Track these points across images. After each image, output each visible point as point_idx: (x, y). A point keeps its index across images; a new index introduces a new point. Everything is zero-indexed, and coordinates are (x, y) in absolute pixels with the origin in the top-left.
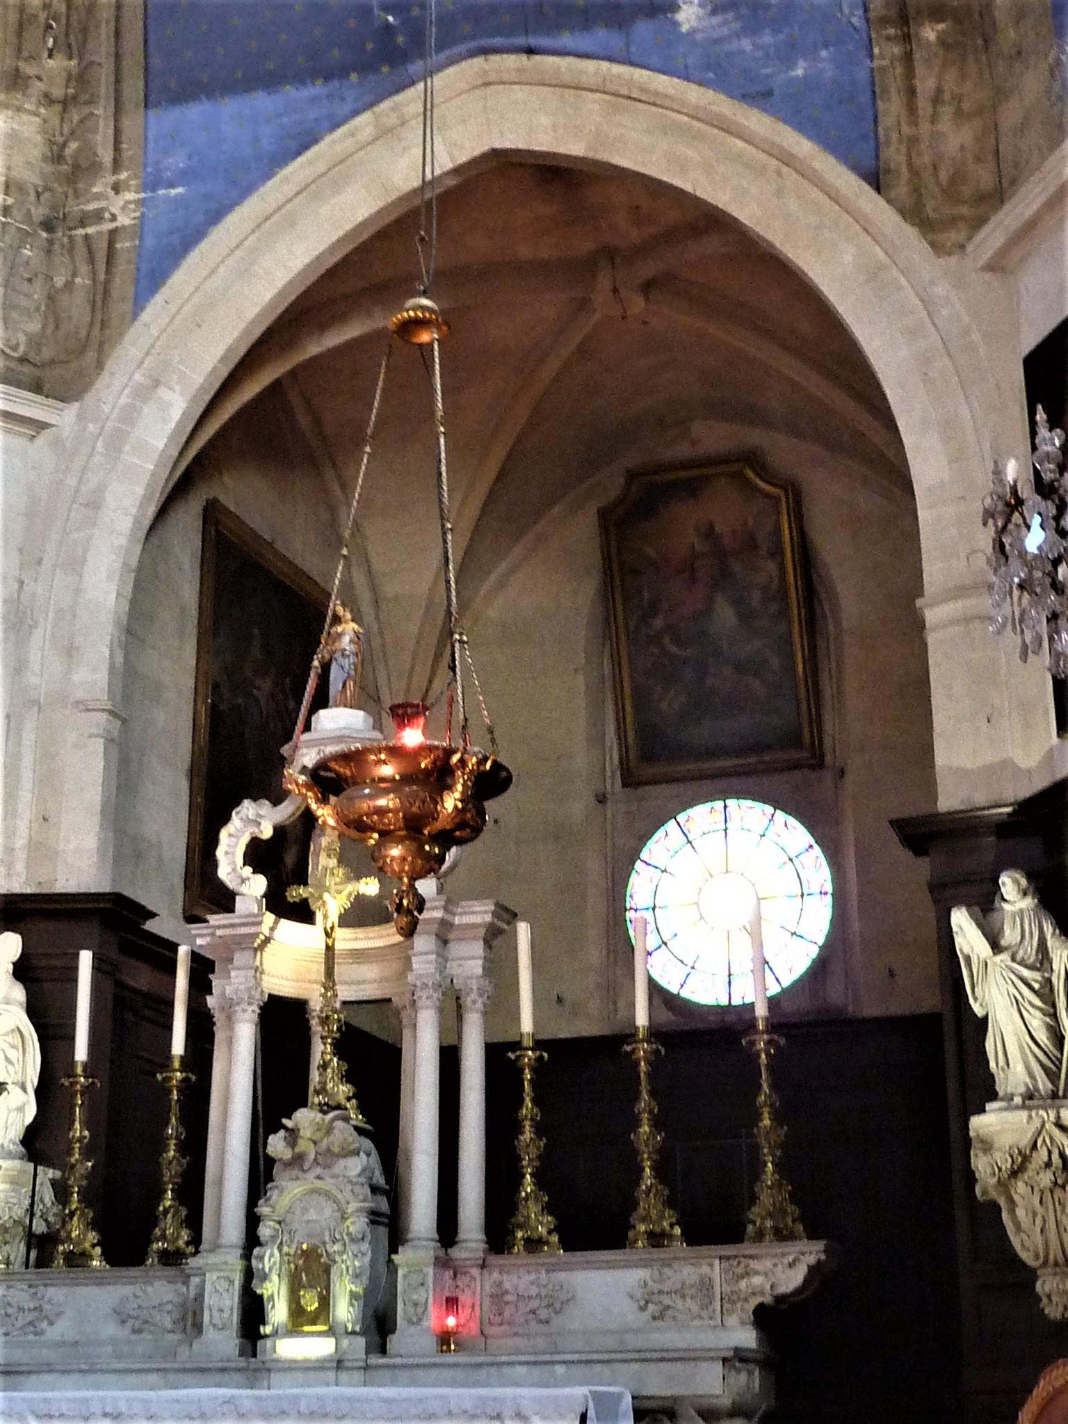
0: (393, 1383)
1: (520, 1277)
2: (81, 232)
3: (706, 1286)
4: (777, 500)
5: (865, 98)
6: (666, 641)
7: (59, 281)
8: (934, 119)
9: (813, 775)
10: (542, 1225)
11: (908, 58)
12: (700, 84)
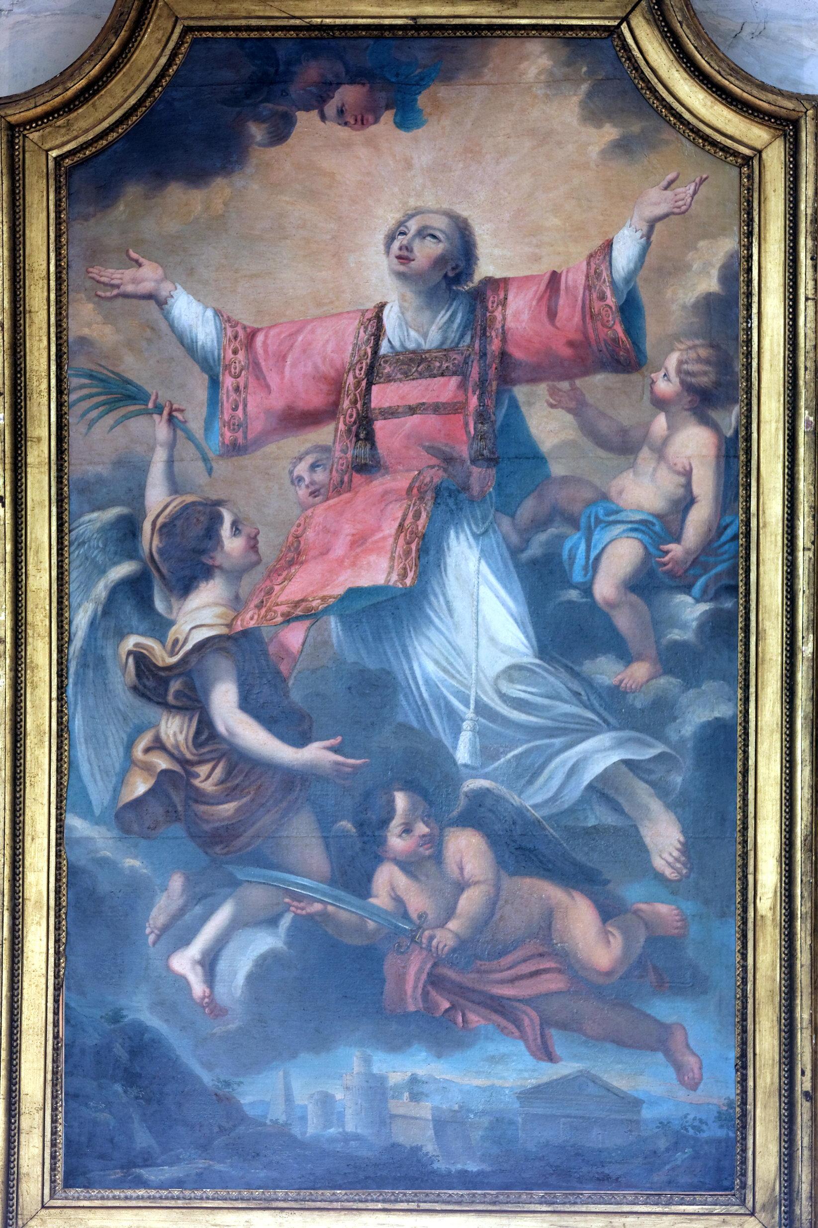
4: (748, 163)
6: (224, 700)
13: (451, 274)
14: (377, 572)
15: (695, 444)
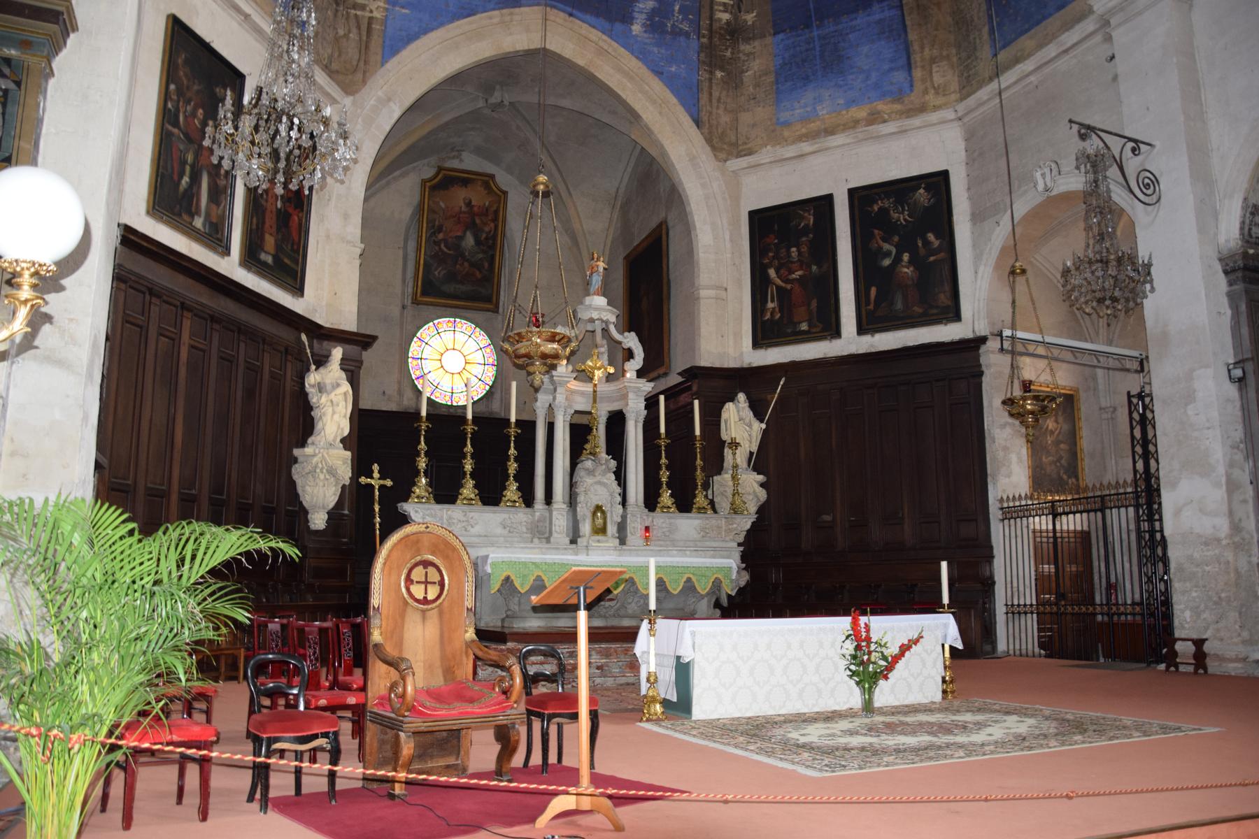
0: (638, 555)
1: (659, 520)
2: (353, 12)
3: (719, 527)
5: (695, 89)
7: (341, 32)
8: (718, 108)
9: (494, 315)
10: (666, 497)
11: (710, 80)
12: (637, 58)
13: (469, 204)
14: (459, 234)
15: (492, 225)
